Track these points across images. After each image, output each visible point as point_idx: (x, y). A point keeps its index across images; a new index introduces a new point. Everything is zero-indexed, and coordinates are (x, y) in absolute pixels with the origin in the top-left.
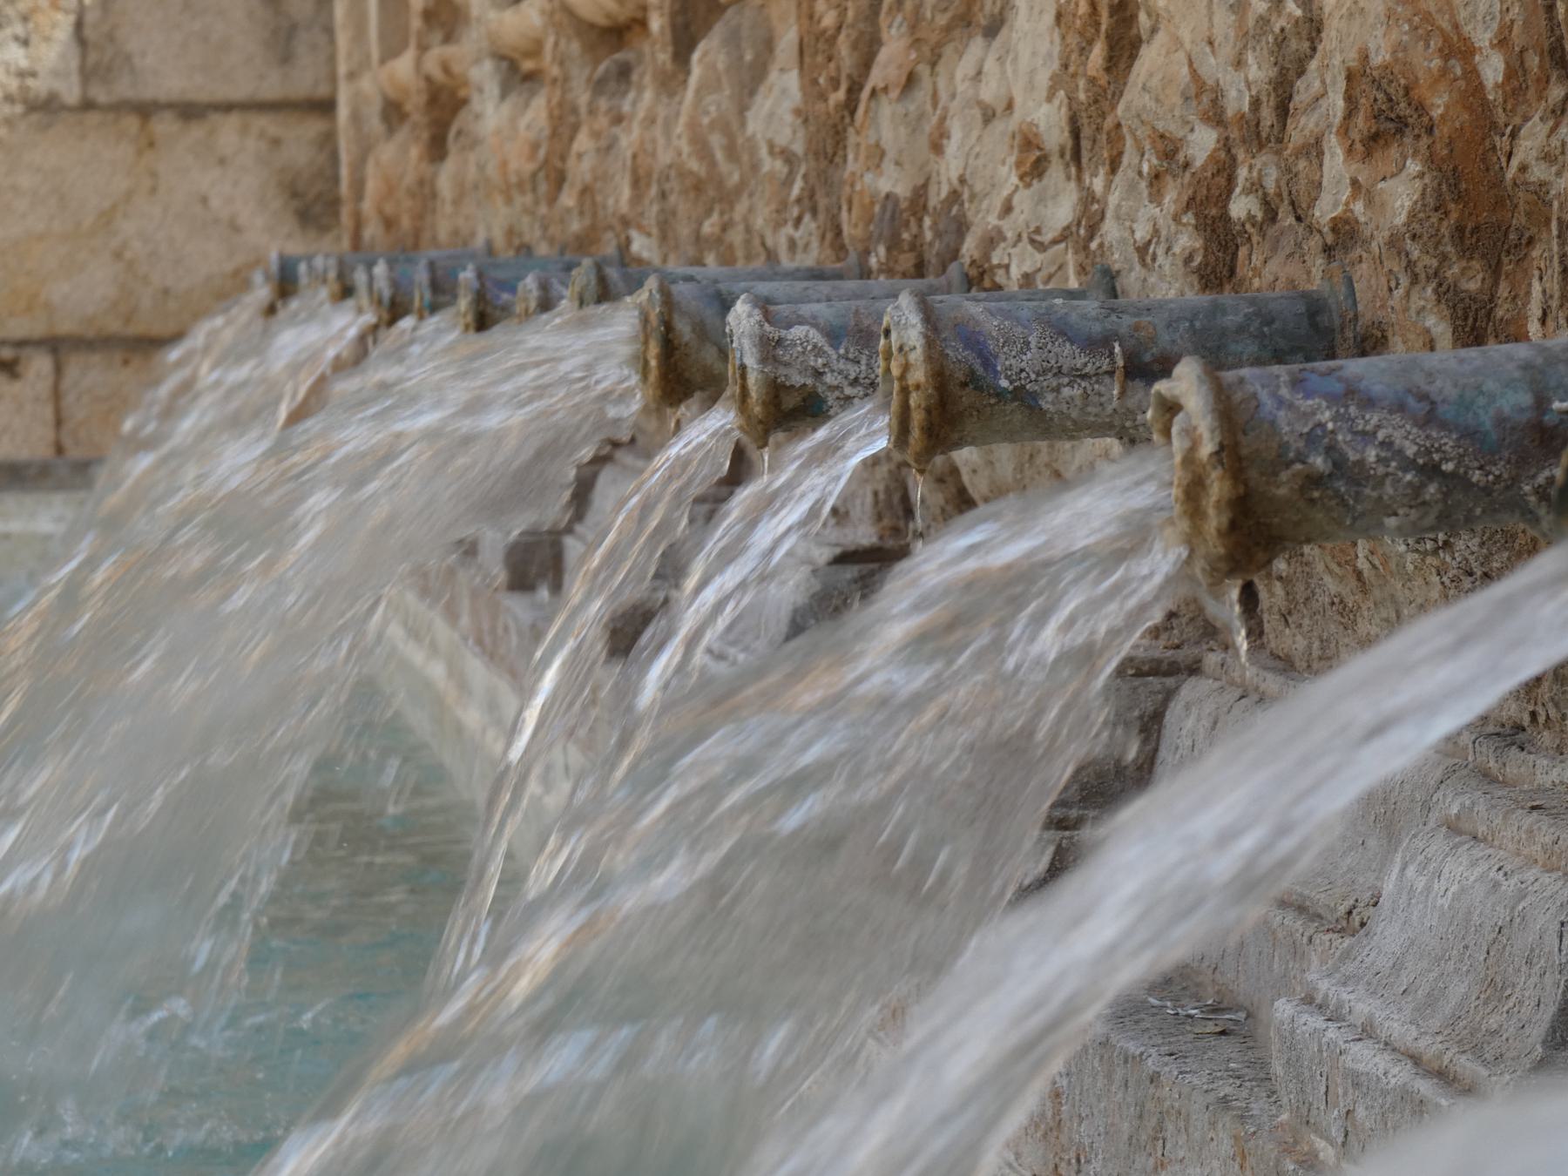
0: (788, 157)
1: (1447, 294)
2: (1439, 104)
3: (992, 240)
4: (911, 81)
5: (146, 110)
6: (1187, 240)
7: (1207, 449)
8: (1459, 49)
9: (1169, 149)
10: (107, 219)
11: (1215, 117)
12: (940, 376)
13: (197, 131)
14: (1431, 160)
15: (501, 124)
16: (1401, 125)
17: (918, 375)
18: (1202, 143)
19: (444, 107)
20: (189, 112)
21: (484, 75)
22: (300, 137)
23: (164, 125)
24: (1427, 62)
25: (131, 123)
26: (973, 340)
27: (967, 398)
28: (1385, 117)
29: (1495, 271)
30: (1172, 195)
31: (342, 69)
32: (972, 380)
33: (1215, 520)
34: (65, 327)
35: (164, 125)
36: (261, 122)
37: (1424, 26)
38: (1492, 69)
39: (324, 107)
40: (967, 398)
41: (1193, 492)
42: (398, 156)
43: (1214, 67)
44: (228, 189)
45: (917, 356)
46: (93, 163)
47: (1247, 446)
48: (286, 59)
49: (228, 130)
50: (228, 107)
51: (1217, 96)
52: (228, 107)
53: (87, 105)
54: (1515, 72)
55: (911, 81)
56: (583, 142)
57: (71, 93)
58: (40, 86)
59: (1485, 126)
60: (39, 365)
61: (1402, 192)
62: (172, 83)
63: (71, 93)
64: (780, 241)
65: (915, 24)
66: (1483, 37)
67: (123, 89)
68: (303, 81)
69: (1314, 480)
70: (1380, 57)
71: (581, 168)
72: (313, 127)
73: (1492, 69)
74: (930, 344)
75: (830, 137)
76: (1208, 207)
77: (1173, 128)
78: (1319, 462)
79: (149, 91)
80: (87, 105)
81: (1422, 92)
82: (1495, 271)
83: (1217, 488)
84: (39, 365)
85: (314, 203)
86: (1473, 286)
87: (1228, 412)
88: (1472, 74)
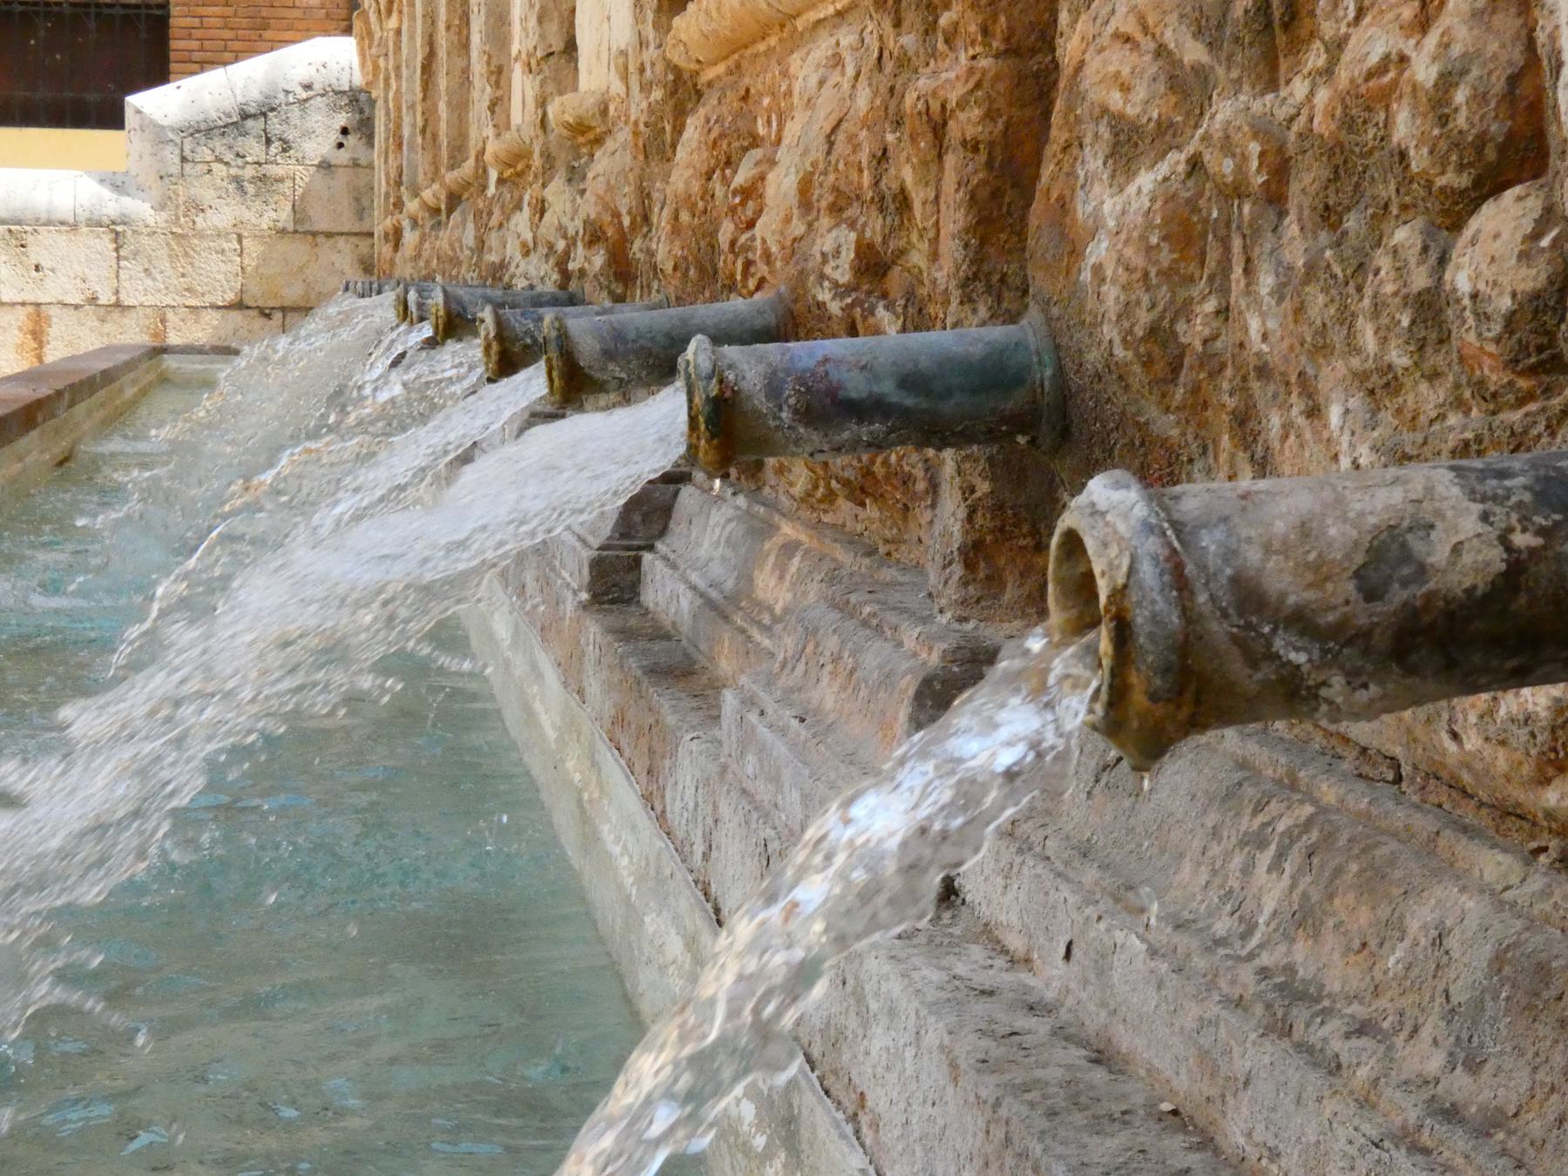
0: (471, 250)
1: (611, 293)
2: (610, 232)
3: (512, 277)
4: (501, 226)
5: (314, 234)
6: (555, 276)
7: (492, 335)
8: (617, 215)
9: (551, 247)
10: (301, 269)
11: (565, 237)
12: (448, 313)
13: (332, 241)
14: (608, 251)
15: (410, 237)
16: (599, 239)
17: (441, 313)
18: (561, 245)
19: (398, 233)
20: (329, 235)
21: (406, 224)
22: (364, 245)
23: (320, 239)
24: (607, 218)
25: (310, 238)
26: (460, 302)
27: (458, 321)
28: (594, 236)
29: (626, 287)
30: (552, 261)
31: (13, 228)
32: (459, 315)
33: (494, 358)
34: (287, 303)
35: (320, 239)
36: (353, 239)
37: (606, 207)
38: (626, 221)
39: (371, 235)
40: (458, 321)
41: (487, 348)
42: (387, 250)
43: (565, 221)
44: (342, 259)
45: (441, 307)
46: (297, 251)
47: (506, 334)
48: (361, 219)
49: (341, 242)
50: (342, 234)
51: (566, 229)
52: (342, 234)
53: (296, 232)
54: (633, 223)
55: (501, 226)
56: (427, 245)
57: (290, 227)
58: (280, 225)
59: (624, 240)
60: (278, 316)
61: (599, 260)
62: (323, 225)
63: (290, 227)
64: (468, 277)
65: (502, 207)
66: (624, 211)
67: (307, 227)
68: (365, 227)
69: (527, 347)
70: (593, 216)
71: (425, 254)
72: (369, 241)
73: (626, 221)
74: (446, 303)
75: (481, 246)
76: (562, 266)
77: (552, 239)
78: (528, 341)
79: (316, 228)
80: (296, 232)
81: (605, 228)
82: (626, 287)
83: (495, 347)
84: (278, 316)
85: (367, 266)
86: (619, 291)
87: (499, 323)
88: (620, 223)
